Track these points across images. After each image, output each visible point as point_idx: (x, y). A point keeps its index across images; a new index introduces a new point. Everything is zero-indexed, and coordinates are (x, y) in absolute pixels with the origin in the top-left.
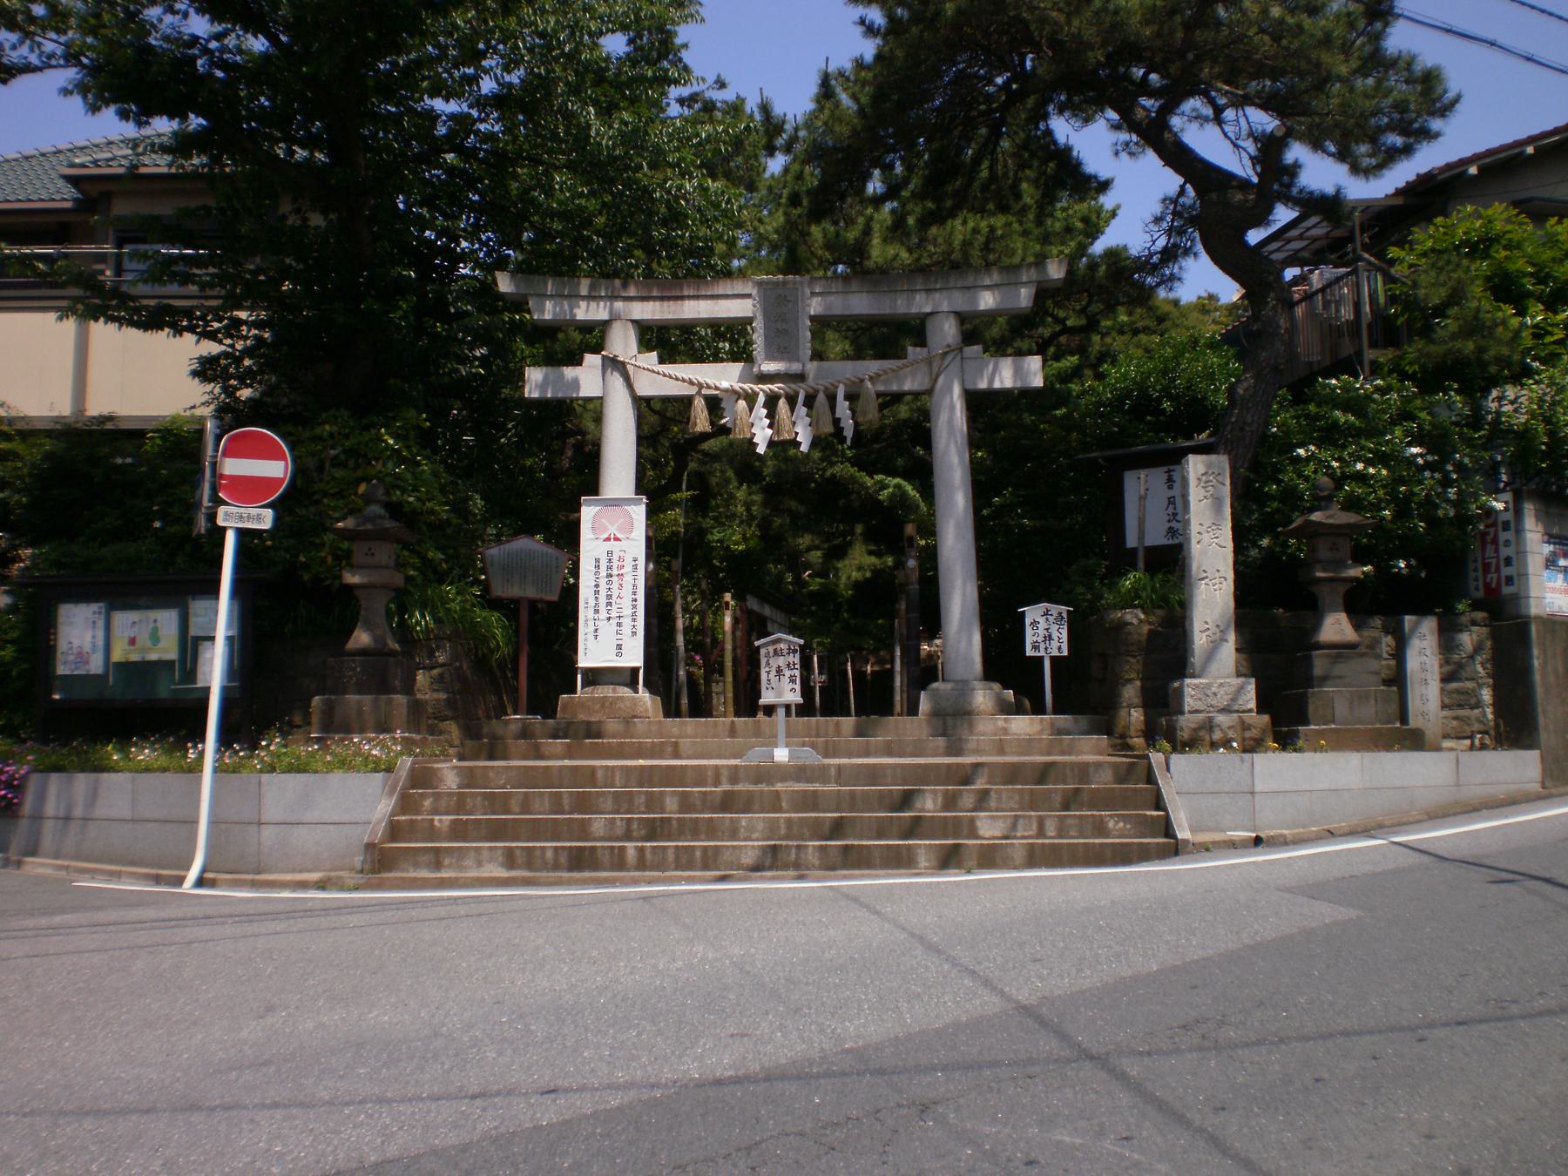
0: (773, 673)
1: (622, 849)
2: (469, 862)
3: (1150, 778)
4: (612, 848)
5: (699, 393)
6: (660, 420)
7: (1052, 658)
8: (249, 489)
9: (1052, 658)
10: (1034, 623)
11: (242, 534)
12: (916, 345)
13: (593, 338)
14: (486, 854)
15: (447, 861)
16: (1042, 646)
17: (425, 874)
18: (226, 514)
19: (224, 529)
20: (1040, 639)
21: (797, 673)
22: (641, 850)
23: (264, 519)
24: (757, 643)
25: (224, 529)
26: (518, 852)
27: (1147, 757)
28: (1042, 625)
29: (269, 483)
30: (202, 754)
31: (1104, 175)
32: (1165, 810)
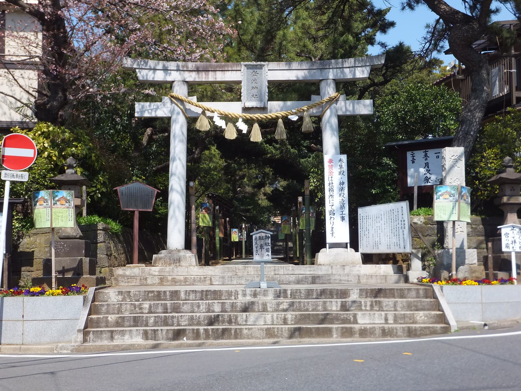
0: (259, 247)
1: (198, 330)
2: (127, 337)
3: (435, 297)
4: (193, 330)
5: (204, 113)
6: (346, 123)
7: (517, 253)
8: (18, 163)
9: (517, 253)
10: (507, 234)
11: (13, 183)
12: (197, 98)
13: (163, 88)
14: (134, 333)
15: (116, 337)
16: (511, 246)
17: (106, 342)
18: (6, 174)
19: (5, 181)
20: (510, 242)
21: (270, 247)
22: (205, 330)
23: (24, 176)
24: (251, 234)
25: (5, 181)
26: (150, 332)
27: (431, 286)
28: (511, 235)
29: (27, 160)
30: (149, 330)
31: (383, 7)
32: (443, 311)
